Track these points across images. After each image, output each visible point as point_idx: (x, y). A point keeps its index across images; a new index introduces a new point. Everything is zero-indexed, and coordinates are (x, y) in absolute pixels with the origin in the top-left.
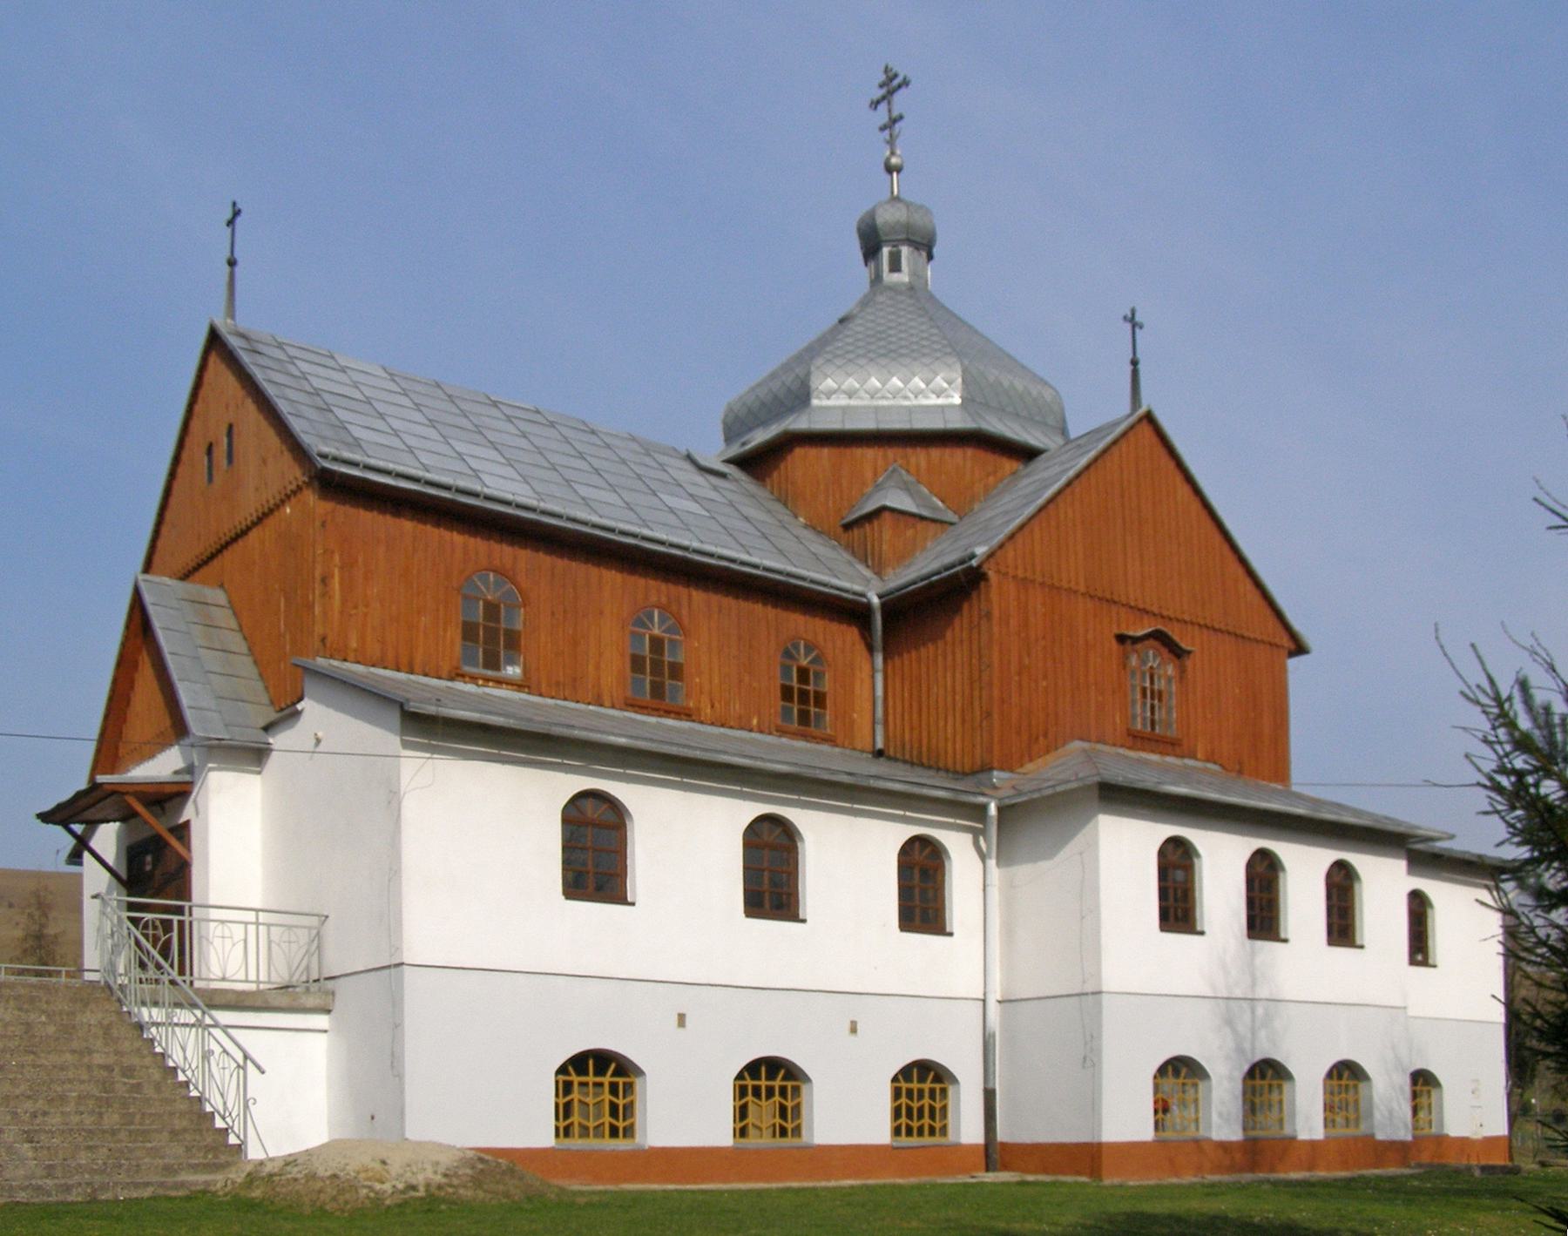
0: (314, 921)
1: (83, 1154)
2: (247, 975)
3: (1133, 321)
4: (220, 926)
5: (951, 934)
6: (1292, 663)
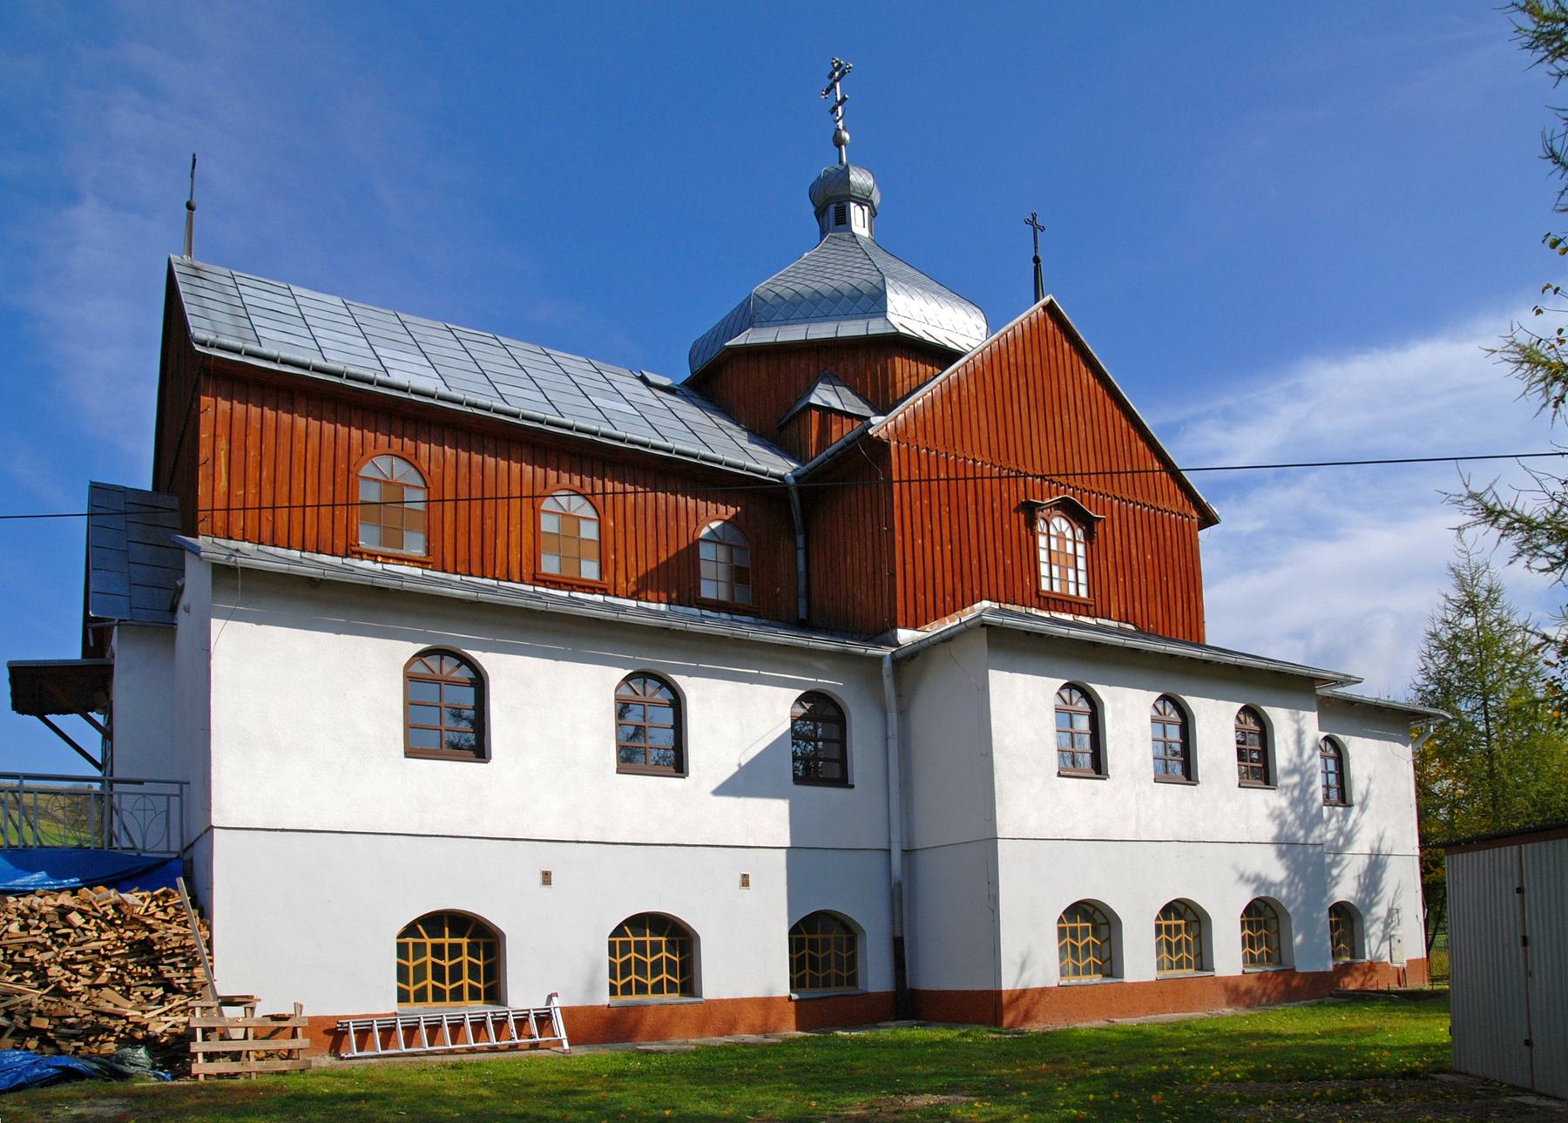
0: (175, 789)
1: (1206, 1055)
2: (169, 846)
3: (1033, 222)
4: (142, 800)
5: (852, 786)
6: (1203, 534)
